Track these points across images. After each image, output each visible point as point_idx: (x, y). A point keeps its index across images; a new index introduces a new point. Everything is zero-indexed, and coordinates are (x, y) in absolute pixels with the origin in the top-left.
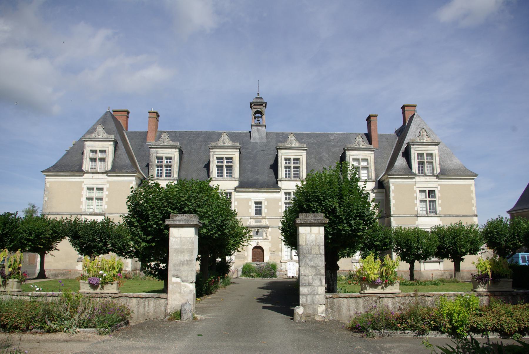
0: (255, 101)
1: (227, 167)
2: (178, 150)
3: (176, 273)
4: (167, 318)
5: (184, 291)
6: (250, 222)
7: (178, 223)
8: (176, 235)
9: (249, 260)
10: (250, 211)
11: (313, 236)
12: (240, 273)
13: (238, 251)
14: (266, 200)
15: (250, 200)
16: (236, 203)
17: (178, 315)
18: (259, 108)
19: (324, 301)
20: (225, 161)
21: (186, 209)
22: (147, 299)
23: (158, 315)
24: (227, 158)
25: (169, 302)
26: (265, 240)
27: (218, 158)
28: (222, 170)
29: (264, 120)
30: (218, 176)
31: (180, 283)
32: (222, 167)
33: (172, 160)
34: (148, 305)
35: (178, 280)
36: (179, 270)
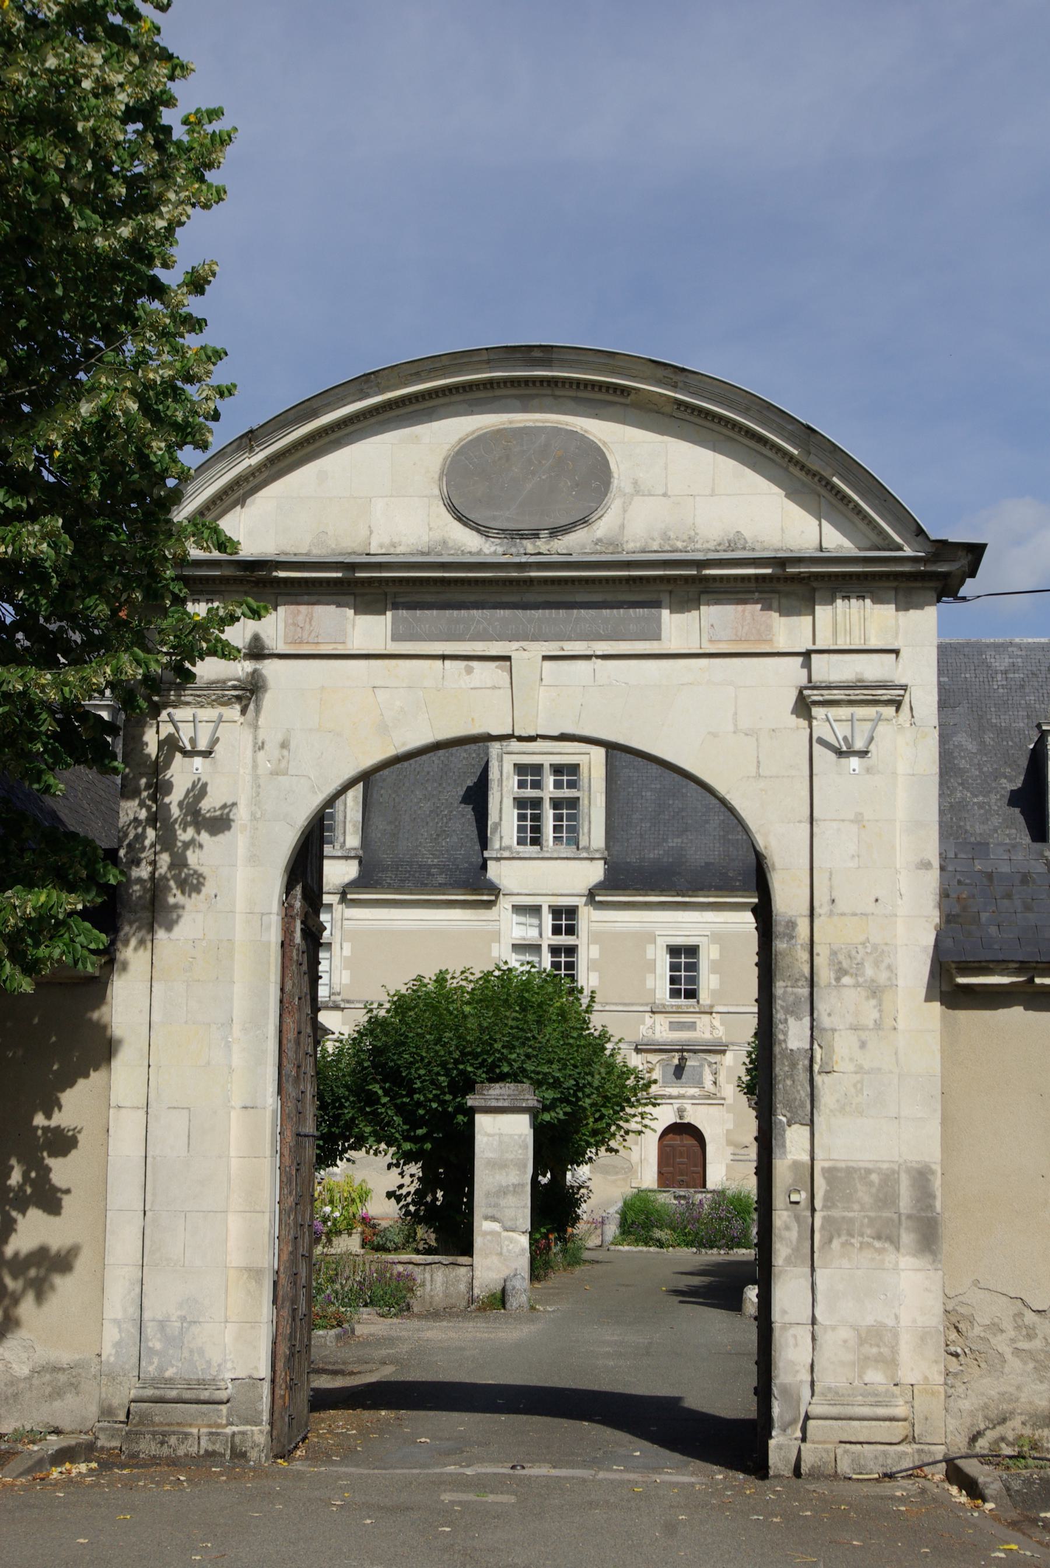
1: (556, 804)
3: (490, 1212)
4: (473, 1307)
5: (509, 1251)
6: (652, 1027)
7: (494, 1103)
8: (490, 1130)
9: (648, 1177)
10: (649, 984)
12: (612, 1230)
13: (610, 1150)
14: (716, 938)
15: (652, 938)
16: (595, 951)
17: (500, 1299)
20: (549, 780)
21: (506, 1069)
22: (428, 1267)
23: (453, 1301)
24: (558, 770)
25: (477, 1273)
26: (711, 1098)
27: (521, 769)
28: (536, 818)
30: (521, 842)
31: (499, 1234)
32: (537, 803)
34: (432, 1281)
35: (496, 1226)
36: (497, 1205)
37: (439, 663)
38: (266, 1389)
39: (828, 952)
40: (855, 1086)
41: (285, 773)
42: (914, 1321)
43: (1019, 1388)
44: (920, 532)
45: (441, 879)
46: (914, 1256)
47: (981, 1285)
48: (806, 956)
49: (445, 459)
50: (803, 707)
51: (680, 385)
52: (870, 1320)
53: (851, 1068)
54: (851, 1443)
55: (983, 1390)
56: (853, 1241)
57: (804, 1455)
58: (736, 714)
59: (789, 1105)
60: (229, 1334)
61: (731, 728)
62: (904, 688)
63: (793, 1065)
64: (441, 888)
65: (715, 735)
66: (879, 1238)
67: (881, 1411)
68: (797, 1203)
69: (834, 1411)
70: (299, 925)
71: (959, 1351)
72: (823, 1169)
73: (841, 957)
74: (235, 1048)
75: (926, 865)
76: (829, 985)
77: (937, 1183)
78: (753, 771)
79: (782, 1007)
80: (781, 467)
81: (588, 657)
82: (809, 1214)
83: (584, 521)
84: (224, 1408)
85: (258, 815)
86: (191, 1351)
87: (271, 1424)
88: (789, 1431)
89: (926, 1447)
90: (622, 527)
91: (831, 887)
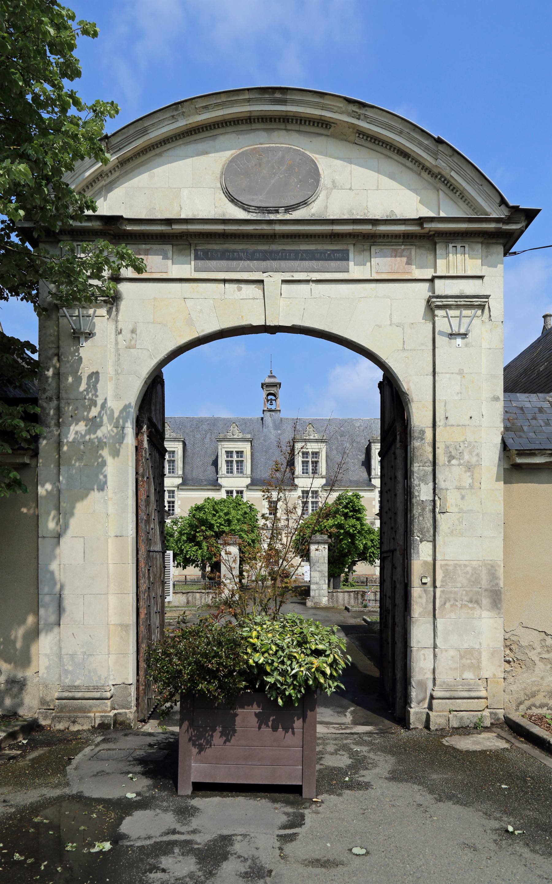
0: (268, 380)
2: (181, 443)
11: (320, 552)
18: (273, 390)
19: (327, 594)
20: (235, 455)
24: (237, 452)
27: (227, 452)
28: (232, 466)
29: (280, 403)
30: (228, 472)
33: (176, 455)
37: (221, 285)
38: (133, 690)
39: (444, 446)
40: (458, 519)
41: (134, 347)
42: (488, 645)
43: (542, 678)
44: (503, 202)
45: (205, 483)
46: (489, 610)
47: (524, 625)
48: (430, 449)
49: (223, 166)
50: (432, 307)
51: (362, 117)
52: (466, 646)
53: (456, 510)
54: (456, 711)
55: (524, 680)
56: (457, 603)
57: (432, 719)
58: (391, 314)
59: (421, 531)
60: (112, 659)
61: (389, 323)
62: (487, 297)
63: (423, 509)
64: (206, 485)
65: (379, 326)
66: (471, 601)
67: (473, 694)
68: (425, 584)
69: (447, 694)
70: (145, 438)
71: (511, 659)
72: (441, 565)
73: (451, 449)
74: (110, 503)
75: (496, 399)
76: (444, 465)
77: (500, 572)
78: (400, 346)
79: (417, 477)
80: (416, 173)
81: (307, 281)
82: (432, 589)
83: (305, 203)
84: (109, 702)
85: (119, 372)
86: (89, 671)
87: (137, 705)
88: (421, 704)
89: (494, 711)
90: (326, 207)
91: (446, 410)
